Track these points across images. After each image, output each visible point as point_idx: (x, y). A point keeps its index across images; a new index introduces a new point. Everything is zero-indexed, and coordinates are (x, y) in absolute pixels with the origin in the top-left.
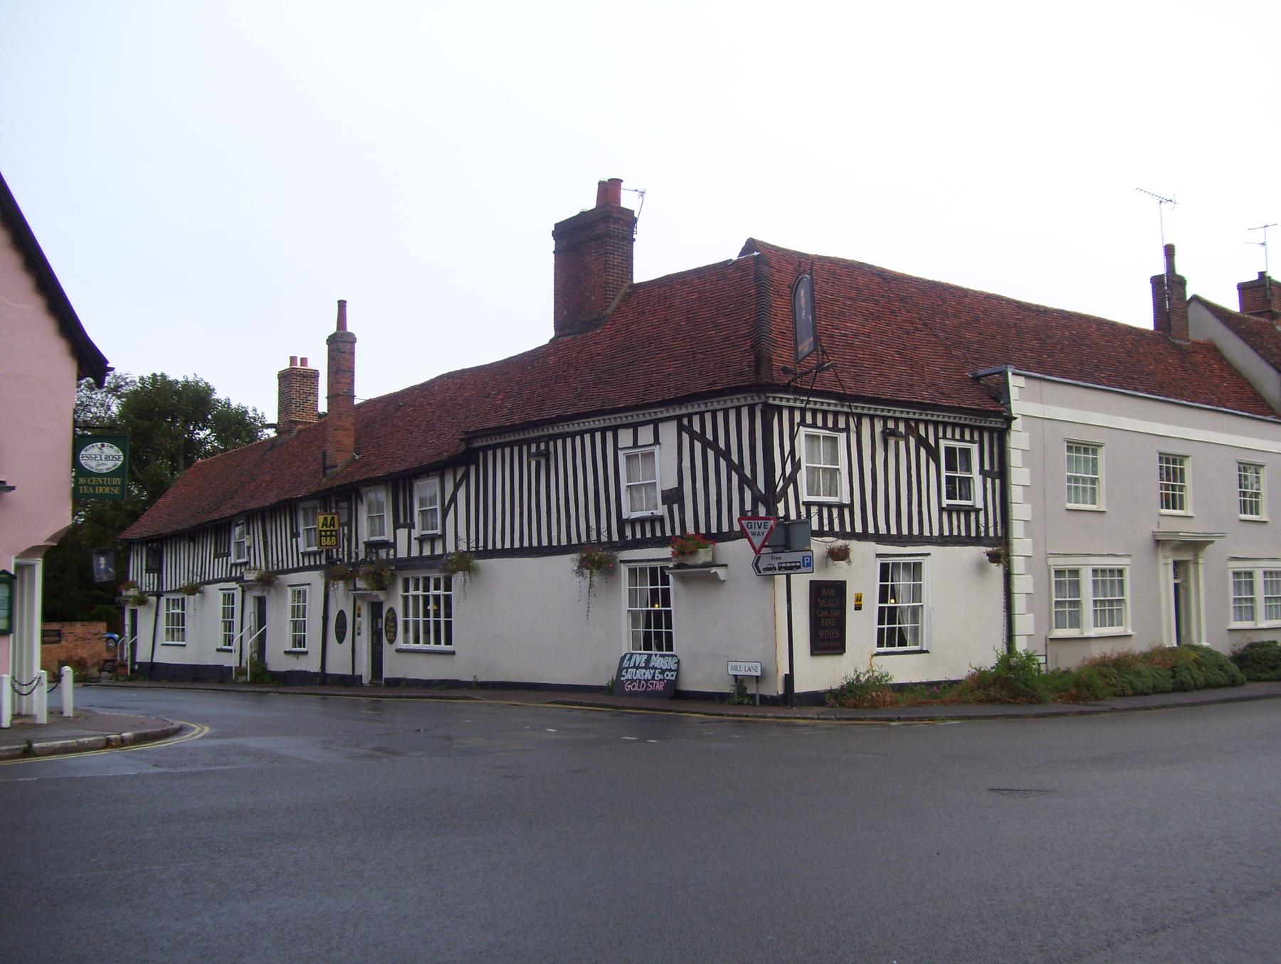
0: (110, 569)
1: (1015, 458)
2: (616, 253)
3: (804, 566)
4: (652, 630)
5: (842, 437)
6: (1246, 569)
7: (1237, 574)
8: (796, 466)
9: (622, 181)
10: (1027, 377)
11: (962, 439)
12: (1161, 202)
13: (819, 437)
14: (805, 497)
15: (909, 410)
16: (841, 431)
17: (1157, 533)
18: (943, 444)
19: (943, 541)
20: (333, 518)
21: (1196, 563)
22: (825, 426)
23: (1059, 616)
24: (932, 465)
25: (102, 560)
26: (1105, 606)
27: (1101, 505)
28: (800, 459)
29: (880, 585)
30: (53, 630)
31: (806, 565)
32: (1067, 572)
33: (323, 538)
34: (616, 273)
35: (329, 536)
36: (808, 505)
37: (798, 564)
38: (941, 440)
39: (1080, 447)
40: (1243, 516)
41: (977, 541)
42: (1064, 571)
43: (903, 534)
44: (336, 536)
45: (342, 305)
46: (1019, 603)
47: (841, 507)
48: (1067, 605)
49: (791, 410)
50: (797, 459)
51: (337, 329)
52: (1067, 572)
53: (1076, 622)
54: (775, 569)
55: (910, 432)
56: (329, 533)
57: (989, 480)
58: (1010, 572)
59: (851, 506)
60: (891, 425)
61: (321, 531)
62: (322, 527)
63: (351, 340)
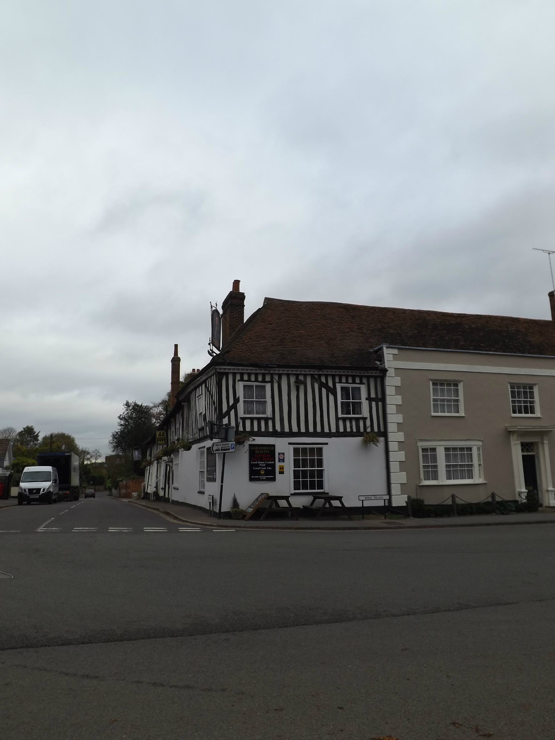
0: (140, 456)
1: (390, 391)
2: (235, 312)
3: (231, 449)
4: (316, 479)
5: (268, 386)
6: (430, 447)
7: (424, 450)
8: (236, 400)
9: (240, 281)
10: (399, 349)
11: (354, 382)
12: (549, 253)
13: (253, 386)
14: (241, 414)
15: (288, 369)
16: (268, 382)
17: (508, 427)
18: (339, 386)
19: (338, 434)
20: (163, 433)
21: (543, 443)
22: (257, 380)
23: (455, 472)
24: (331, 397)
25: (136, 452)
26: (465, 468)
27: (462, 413)
28: (239, 397)
29: (294, 459)
30: (216, 477)
31: (232, 448)
32: (429, 449)
33: (159, 441)
34: (235, 321)
35: (162, 440)
36: (244, 419)
37: (229, 448)
38: (337, 384)
39: (451, 384)
40: (514, 415)
41: (358, 434)
42: (428, 449)
43: (262, 431)
44: (165, 440)
45: (176, 346)
46: (394, 467)
47: (266, 420)
48: (466, 466)
49: (234, 374)
50: (237, 397)
51: (174, 356)
52: (429, 449)
53: (436, 478)
54: (219, 450)
55: (315, 381)
56: (161, 439)
57: (374, 404)
58: (388, 450)
59: (273, 419)
60: (301, 378)
61: (158, 438)
62: (159, 436)
63: (179, 360)
